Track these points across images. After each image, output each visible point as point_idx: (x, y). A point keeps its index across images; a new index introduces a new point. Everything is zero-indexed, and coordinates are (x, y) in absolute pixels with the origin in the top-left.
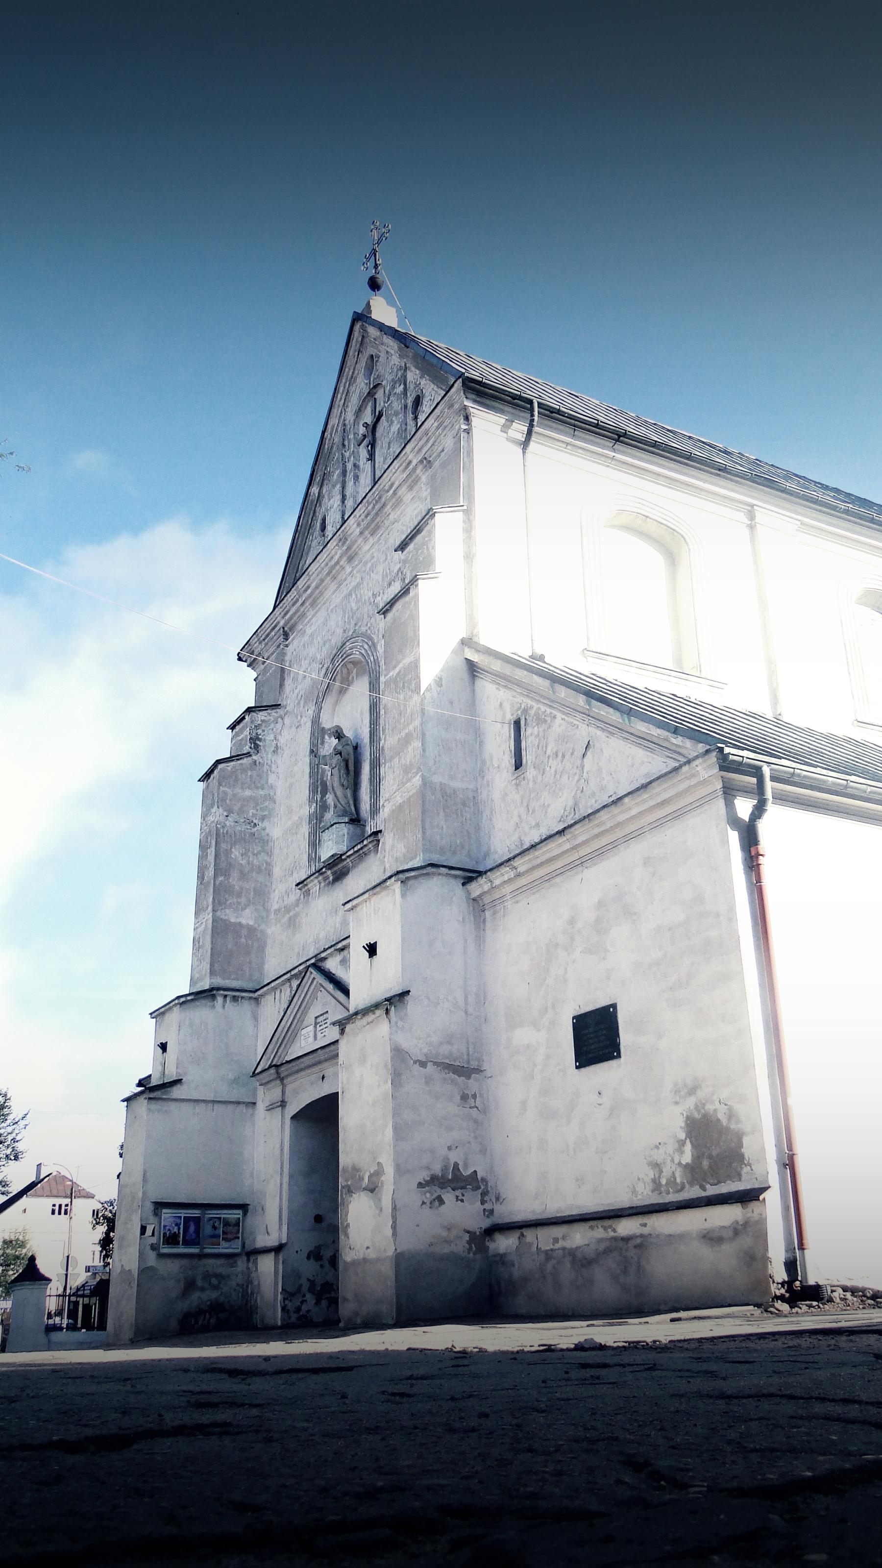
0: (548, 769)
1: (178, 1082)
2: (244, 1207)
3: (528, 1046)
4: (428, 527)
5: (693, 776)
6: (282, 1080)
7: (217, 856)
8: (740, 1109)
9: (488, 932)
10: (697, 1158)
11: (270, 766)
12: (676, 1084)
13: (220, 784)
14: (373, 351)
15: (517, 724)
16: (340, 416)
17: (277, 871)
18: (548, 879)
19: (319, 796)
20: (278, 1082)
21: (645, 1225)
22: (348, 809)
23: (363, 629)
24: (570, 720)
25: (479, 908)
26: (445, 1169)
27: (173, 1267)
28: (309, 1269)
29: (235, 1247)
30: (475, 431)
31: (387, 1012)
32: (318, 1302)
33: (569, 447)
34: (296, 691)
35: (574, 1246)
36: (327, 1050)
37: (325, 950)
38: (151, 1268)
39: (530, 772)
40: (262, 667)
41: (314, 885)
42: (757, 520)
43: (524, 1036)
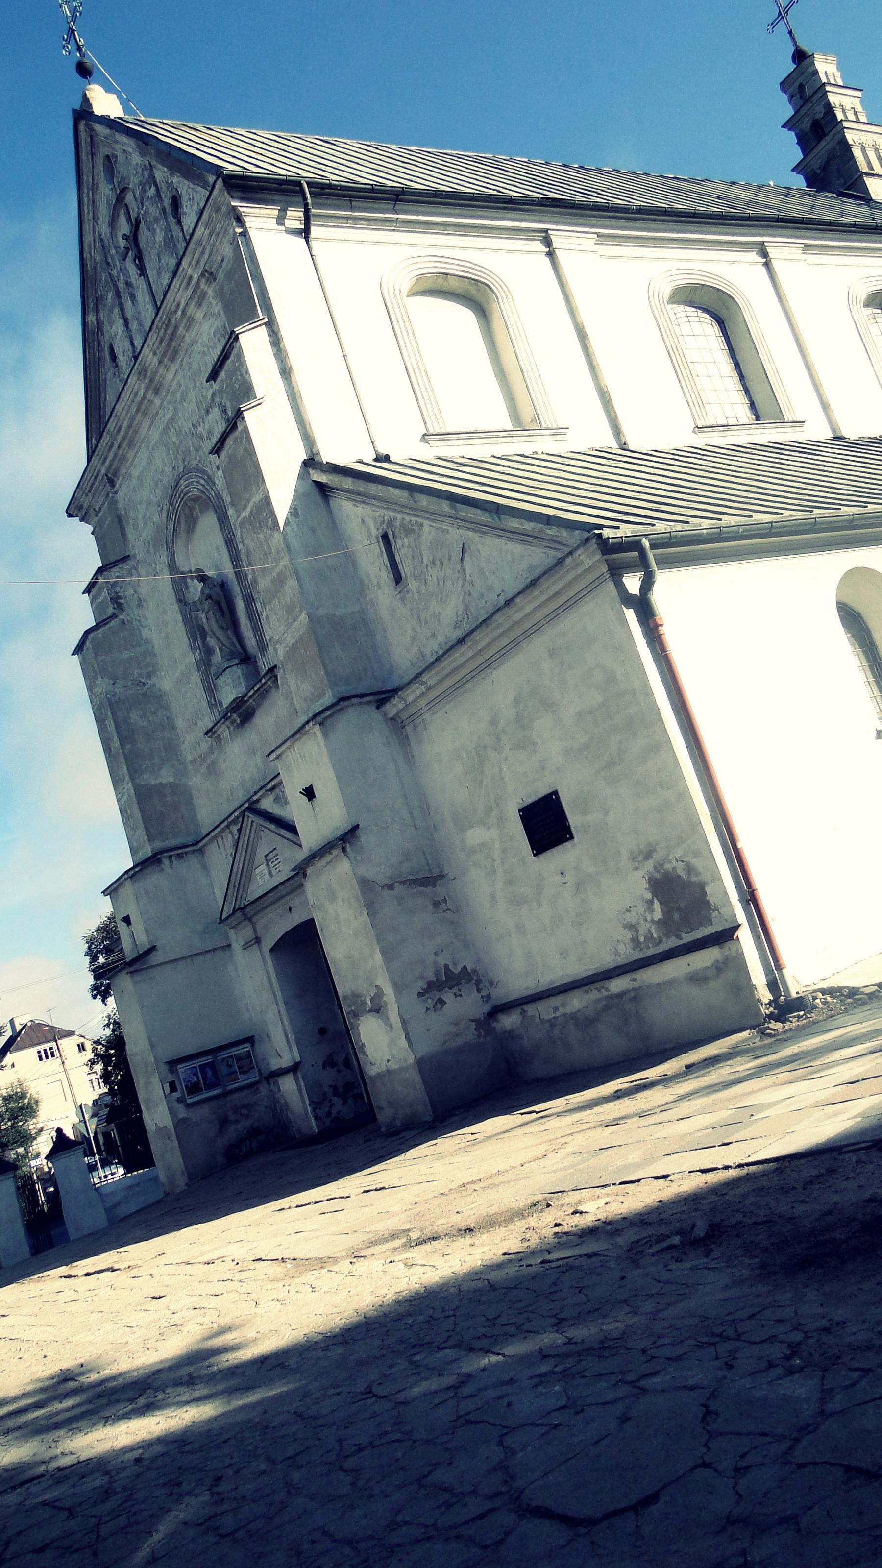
0: (429, 578)
1: (153, 949)
2: (250, 1040)
3: (483, 845)
4: (235, 352)
5: (579, 564)
6: (250, 919)
7: (117, 727)
8: (697, 863)
9: (414, 746)
10: (667, 913)
11: (139, 621)
12: (632, 853)
13: (96, 654)
14: (106, 151)
15: (385, 537)
16: (94, 232)
17: (180, 723)
18: (460, 685)
19: (200, 641)
20: (247, 922)
21: (634, 980)
22: (234, 649)
23: (194, 463)
24: (438, 525)
25: (401, 729)
26: (437, 973)
27: (204, 1111)
28: (327, 1077)
29: (253, 1076)
30: (252, 233)
31: (344, 850)
32: (345, 1102)
33: (350, 221)
34: (141, 539)
35: (574, 1010)
36: (287, 884)
37: (256, 793)
38: (184, 1120)
39: (413, 585)
40: (96, 519)
41: (224, 731)
42: (555, 245)
43: (476, 836)
